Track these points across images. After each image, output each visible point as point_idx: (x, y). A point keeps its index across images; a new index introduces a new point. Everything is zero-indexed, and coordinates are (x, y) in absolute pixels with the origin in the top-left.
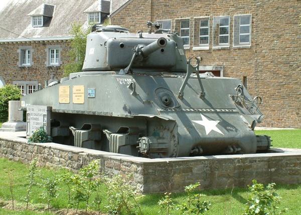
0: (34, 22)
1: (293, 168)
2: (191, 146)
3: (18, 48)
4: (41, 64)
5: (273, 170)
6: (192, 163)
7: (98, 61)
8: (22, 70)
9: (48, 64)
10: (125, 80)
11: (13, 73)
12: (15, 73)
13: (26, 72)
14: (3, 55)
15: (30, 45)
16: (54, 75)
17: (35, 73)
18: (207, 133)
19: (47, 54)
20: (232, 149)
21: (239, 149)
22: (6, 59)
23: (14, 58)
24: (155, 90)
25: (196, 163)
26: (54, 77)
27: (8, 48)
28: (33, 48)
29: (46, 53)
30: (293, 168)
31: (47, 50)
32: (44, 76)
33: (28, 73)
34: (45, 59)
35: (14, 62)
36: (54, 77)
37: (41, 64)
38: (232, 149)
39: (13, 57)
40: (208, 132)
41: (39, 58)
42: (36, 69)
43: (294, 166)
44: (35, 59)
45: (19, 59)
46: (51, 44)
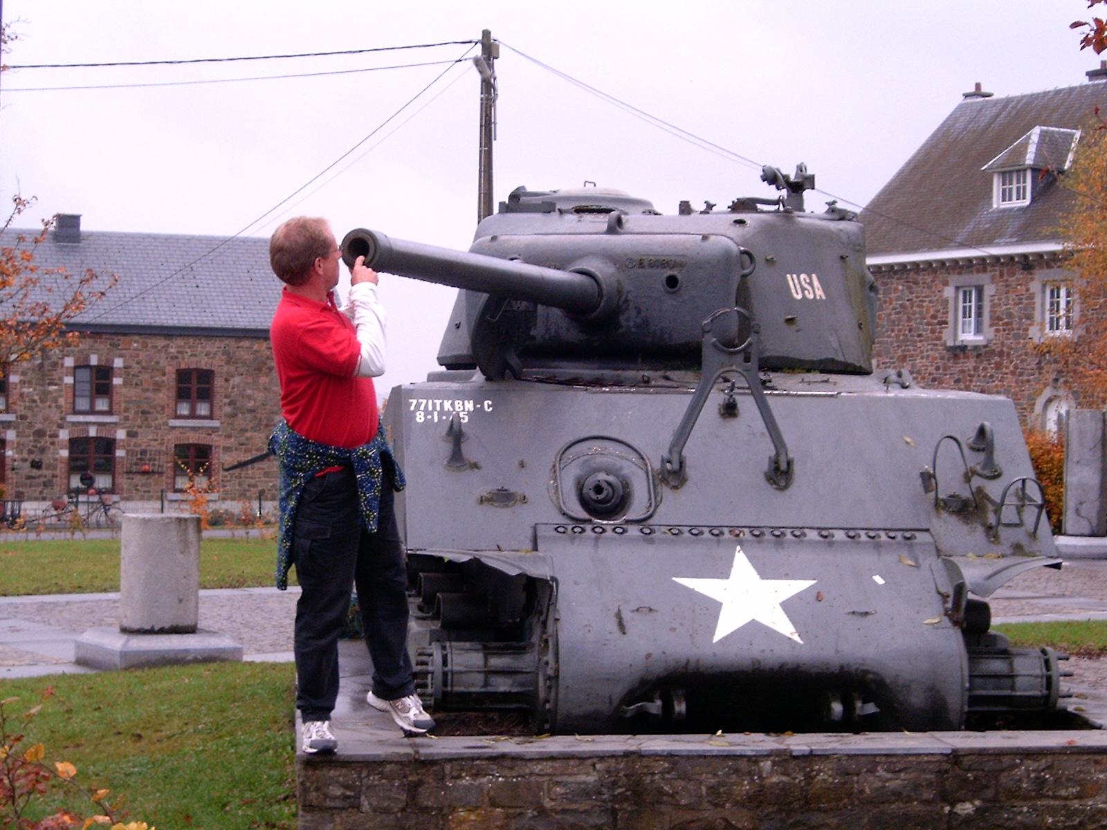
0: (1004, 191)
1: (1076, 804)
2: (619, 691)
3: (946, 284)
4: (1017, 337)
5: (966, 808)
6: (538, 768)
7: (458, 326)
8: (956, 357)
9: (1038, 335)
10: (447, 405)
11: (931, 369)
12: (938, 368)
13: (970, 364)
14: (901, 305)
15: (985, 271)
16: (1060, 372)
17: (998, 366)
18: (719, 634)
19: (1038, 300)
20: (837, 708)
21: (871, 708)
22: (909, 320)
23: (934, 317)
24: (550, 457)
25: (557, 764)
26: (1056, 380)
27: (916, 283)
28: (993, 281)
29: (1031, 297)
30: (1076, 804)
31: (1035, 286)
32: (1025, 378)
33: (975, 368)
34: (1030, 317)
35: (933, 331)
36: (1056, 380)
37: (1017, 337)
38: (837, 708)
39: (932, 312)
40: (725, 627)
41: (1010, 315)
42: (1001, 354)
43: (1079, 796)
44: (999, 319)
45: (950, 318)
46: (1049, 267)
